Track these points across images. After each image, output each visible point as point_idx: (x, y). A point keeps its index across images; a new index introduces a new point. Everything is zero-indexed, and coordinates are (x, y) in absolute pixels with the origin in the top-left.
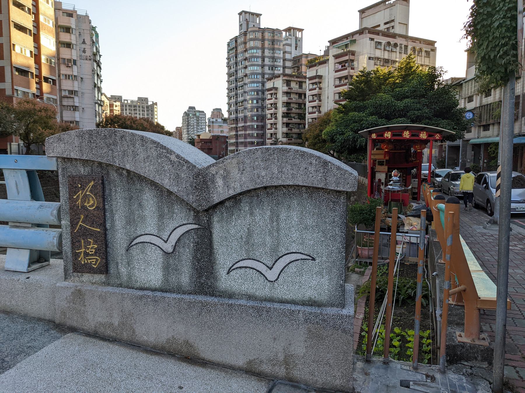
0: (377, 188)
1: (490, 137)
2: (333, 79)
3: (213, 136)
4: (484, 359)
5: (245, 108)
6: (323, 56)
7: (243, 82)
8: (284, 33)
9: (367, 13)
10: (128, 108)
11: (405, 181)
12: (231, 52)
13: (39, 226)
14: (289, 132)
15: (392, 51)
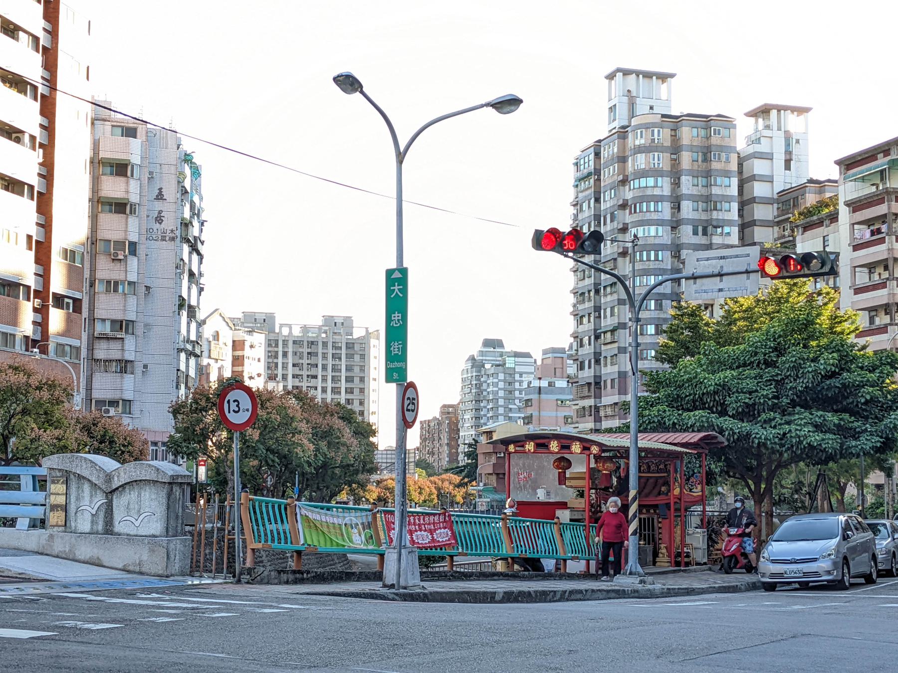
4: (248, 574)
12: (583, 186)
13: (35, 505)
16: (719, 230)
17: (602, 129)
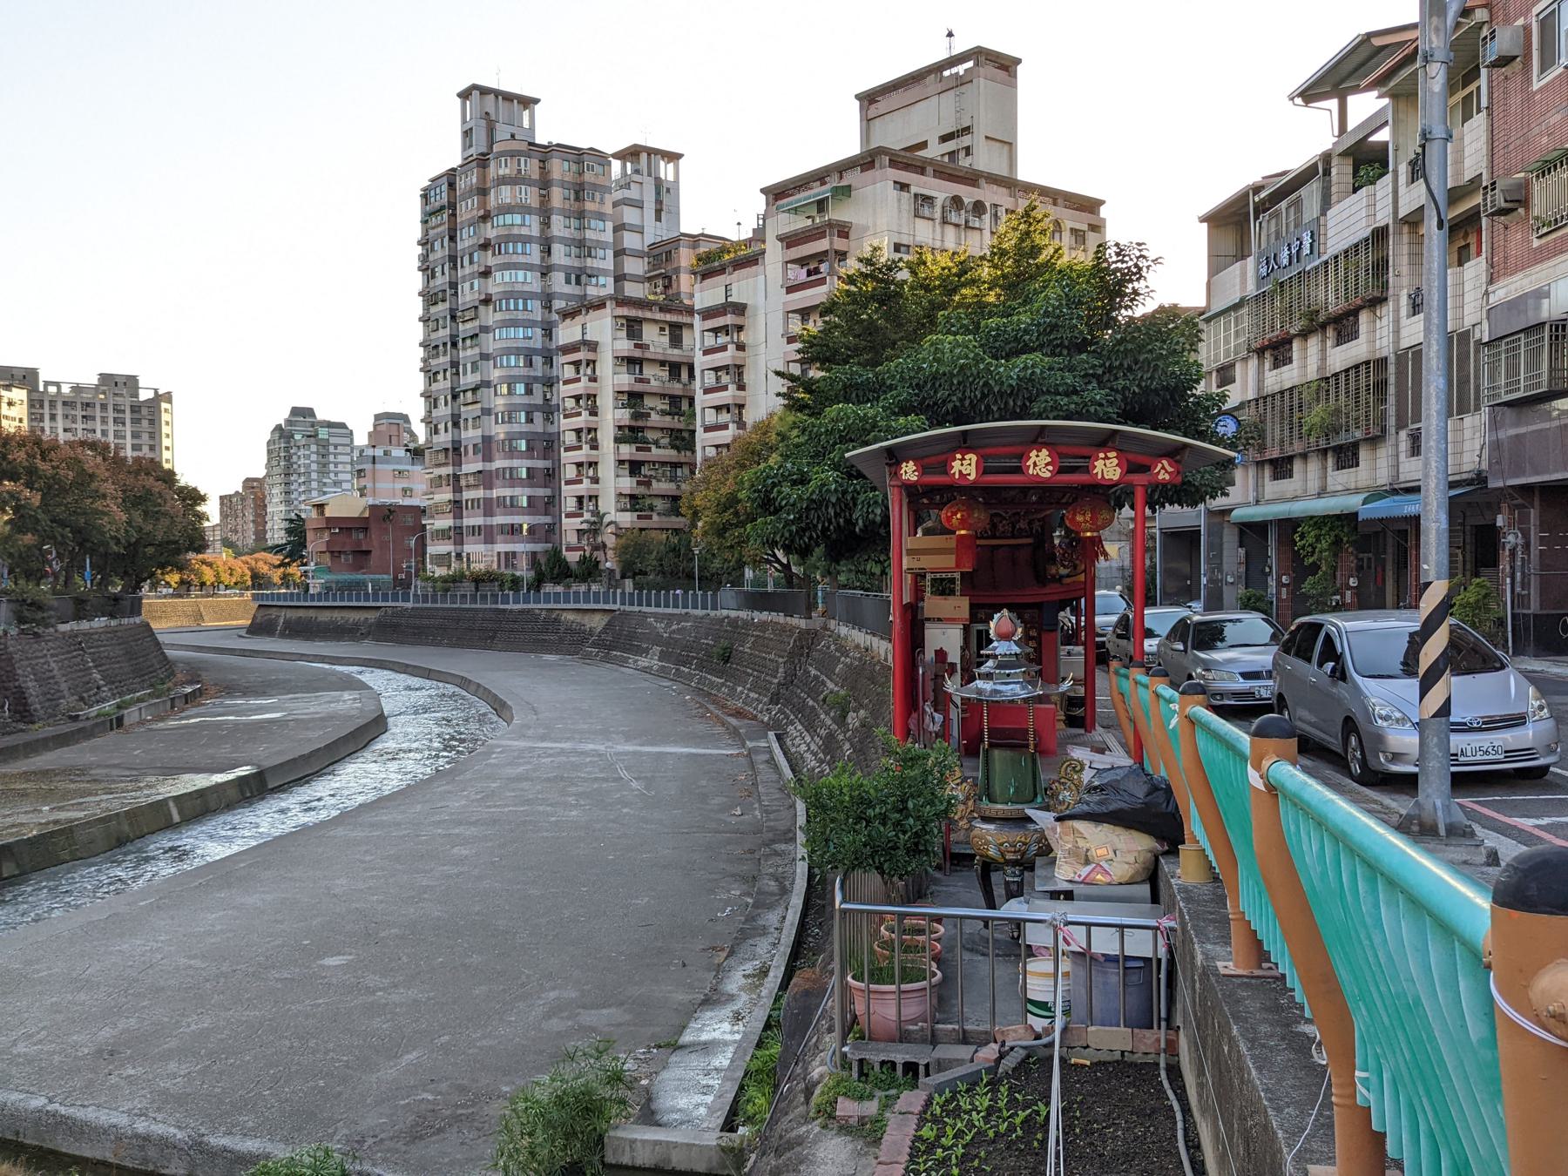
0: (930, 686)
1: (1295, 498)
2: (780, 315)
3: (373, 508)
5: (487, 412)
6: (748, 243)
7: (476, 323)
8: (616, 165)
9: (882, 105)
10: (60, 411)
11: (1039, 661)
12: (434, 221)
14: (642, 490)
15: (967, 227)
16: (594, 280)
17: (452, 157)
